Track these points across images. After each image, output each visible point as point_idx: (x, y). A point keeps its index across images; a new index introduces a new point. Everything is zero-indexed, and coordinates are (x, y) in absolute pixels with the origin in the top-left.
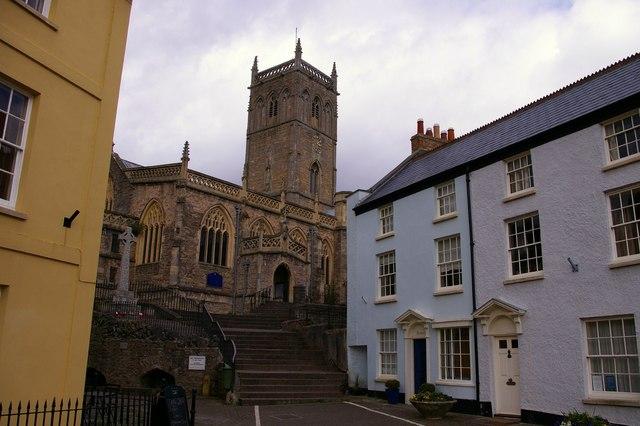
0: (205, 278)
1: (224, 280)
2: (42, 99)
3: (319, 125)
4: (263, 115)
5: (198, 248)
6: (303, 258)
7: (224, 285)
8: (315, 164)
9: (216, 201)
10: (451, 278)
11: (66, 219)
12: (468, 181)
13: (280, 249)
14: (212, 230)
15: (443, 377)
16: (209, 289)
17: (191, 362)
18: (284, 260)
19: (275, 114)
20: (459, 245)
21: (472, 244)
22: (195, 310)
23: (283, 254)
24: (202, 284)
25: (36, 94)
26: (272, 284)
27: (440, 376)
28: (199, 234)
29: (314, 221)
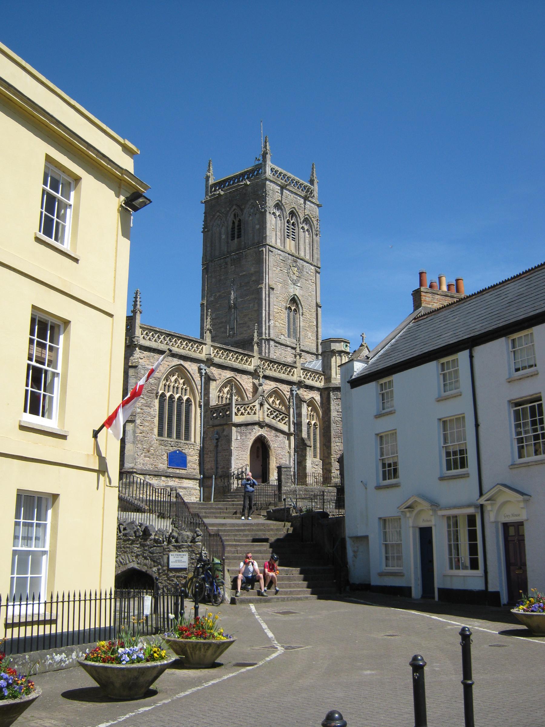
1: (189, 458)
2: (73, 327)
3: (298, 248)
4: (223, 237)
5: (156, 420)
6: (285, 428)
8: (294, 300)
9: (176, 362)
10: (456, 460)
11: (94, 431)
12: (471, 357)
13: (256, 418)
14: (171, 397)
15: (451, 568)
16: (170, 470)
17: (172, 559)
18: (258, 432)
19: (239, 236)
20: (464, 426)
21: (477, 425)
22: (167, 499)
23: (261, 425)
24: (163, 465)
25: (67, 323)
27: (156, 431)
28: (156, 402)
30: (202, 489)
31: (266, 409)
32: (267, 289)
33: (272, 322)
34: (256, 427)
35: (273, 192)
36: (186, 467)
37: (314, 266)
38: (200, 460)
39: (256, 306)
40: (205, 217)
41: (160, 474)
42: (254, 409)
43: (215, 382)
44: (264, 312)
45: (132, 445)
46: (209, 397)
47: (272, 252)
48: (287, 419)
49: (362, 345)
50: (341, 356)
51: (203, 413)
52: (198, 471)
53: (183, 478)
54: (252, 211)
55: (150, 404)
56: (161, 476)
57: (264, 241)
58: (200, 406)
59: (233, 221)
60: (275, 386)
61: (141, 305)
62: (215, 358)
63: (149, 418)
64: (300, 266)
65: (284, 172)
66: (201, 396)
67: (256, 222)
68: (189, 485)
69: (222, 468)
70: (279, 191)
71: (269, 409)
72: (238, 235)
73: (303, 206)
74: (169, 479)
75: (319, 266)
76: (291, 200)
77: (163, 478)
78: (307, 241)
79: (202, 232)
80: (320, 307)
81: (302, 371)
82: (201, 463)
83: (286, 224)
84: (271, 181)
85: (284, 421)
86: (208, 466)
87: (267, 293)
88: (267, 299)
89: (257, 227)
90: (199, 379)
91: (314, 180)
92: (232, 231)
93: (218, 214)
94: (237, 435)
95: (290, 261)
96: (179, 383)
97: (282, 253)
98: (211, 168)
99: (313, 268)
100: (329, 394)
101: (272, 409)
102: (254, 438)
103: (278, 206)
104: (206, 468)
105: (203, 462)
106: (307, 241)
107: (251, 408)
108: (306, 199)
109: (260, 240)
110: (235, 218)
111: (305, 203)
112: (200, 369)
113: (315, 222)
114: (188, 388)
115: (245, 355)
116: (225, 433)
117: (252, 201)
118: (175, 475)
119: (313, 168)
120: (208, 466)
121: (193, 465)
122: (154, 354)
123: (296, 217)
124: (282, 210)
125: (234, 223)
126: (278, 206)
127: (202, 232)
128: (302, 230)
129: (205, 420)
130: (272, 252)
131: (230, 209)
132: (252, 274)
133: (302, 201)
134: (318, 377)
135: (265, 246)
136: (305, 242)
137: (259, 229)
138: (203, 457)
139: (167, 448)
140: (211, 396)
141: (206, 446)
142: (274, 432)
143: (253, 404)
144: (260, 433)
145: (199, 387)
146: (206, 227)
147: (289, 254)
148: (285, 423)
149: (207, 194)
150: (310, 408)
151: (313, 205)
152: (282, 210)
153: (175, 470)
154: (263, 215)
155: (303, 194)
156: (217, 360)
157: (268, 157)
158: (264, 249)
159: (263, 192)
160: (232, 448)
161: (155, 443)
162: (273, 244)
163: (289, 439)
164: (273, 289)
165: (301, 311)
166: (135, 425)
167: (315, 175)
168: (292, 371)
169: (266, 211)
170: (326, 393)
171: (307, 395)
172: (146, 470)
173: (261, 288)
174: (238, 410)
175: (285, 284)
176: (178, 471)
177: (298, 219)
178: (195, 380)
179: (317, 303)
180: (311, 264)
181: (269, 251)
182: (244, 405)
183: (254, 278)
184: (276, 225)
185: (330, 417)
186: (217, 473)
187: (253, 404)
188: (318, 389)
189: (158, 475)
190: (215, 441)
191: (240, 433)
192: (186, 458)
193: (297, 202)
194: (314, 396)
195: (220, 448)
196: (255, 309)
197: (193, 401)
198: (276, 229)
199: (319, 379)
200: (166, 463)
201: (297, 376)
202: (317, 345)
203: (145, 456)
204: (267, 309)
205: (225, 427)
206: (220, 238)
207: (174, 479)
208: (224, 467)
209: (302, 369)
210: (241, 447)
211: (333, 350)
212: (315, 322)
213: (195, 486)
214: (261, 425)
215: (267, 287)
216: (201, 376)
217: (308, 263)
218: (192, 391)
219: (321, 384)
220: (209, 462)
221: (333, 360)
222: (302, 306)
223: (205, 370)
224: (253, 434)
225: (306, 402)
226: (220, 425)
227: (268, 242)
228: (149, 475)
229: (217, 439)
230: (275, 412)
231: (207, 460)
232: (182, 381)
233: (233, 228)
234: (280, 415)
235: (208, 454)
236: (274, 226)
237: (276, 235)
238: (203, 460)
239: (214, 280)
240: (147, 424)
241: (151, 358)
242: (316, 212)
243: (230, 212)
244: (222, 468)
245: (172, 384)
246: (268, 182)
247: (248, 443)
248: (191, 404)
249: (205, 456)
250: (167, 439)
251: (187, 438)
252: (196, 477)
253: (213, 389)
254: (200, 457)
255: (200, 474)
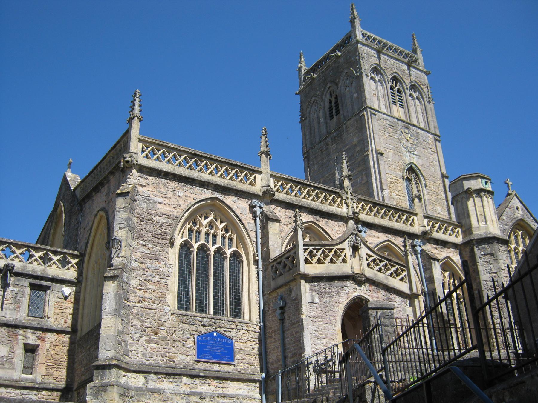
0: (190, 343)
1: (237, 346)
4: (322, 120)
5: (173, 282)
6: (404, 287)
7: (238, 357)
9: (208, 194)
16: (200, 366)
18: (352, 291)
19: (338, 113)
23: (358, 280)
24: (185, 356)
26: (339, 339)
27: (172, 299)
28: (173, 256)
29: (416, 229)
30: (264, 396)
31: (364, 256)
32: (375, 155)
33: (386, 192)
34: (349, 283)
35: (368, 57)
36: (233, 360)
37: (432, 134)
38: (260, 349)
39: (365, 178)
40: (301, 106)
41: (178, 371)
42: (343, 254)
43: (277, 224)
44: (374, 181)
45: (112, 318)
46: (268, 247)
47: (375, 115)
48: (405, 273)
49: (509, 194)
50: (481, 197)
51: (261, 273)
52: (258, 368)
53: (226, 379)
54: (348, 81)
55: (159, 255)
56: (180, 375)
57: (363, 104)
58: (256, 262)
59: (330, 100)
60: (385, 239)
61: (140, 111)
62: (276, 193)
63: (157, 278)
64: (414, 133)
65: (379, 38)
66: (257, 247)
67: (354, 91)
68: (240, 392)
69: (292, 357)
70: (376, 56)
71: (370, 256)
72: (336, 112)
73: (407, 72)
74: (197, 381)
75: (438, 133)
76: (390, 65)
77: (185, 379)
78: (419, 110)
79: (300, 123)
80: (447, 178)
81: (425, 220)
82: (263, 355)
83: (390, 91)
84: (364, 45)
85: (400, 277)
86: (274, 356)
87: (375, 159)
88: (376, 166)
89: (356, 95)
90: (253, 222)
91: (416, 49)
92: (330, 111)
93: (314, 98)
94: (312, 296)
95: (400, 127)
96: (217, 228)
97: (389, 118)
98: (303, 60)
99: (431, 136)
100: (472, 250)
101: (375, 256)
102: (347, 301)
103: (376, 70)
104: (271, 360)
105: (266, 352)
106: (419, 110)
107: (336, 252)
108: (409, 66)
109: (361, 104)
110: (331, 97)
111: (409, 69)
112: (252, 207)
113: (425, 90)
114: (235, 237)
115: (330, 192)
116: (293, 295)
117: (346, 71)
118: (213, 374)
119: (413, 39)
120: (274, 356)
121: (247, 357)
122: (166, 181)
123: (401, 83)
124: (381, 74)
125: (330, 102)
126: (376, 70)
127: (300, 123)
128: (410, 98)
129: (266, 282)
130: (375, 115)
131: (325, 88)
132: (356, 145)
133: (405, 67)
134: (452, 230)
135: (365, 109)
136: (416, 110)
137: (358, 98)
138: (265, 343)
139: (194, 328)
140: (270, 244)
141: (267, 323)
142: (383, 292)
143: (340, 247)
144: (357, 294)
145: (252, 234)
146: (303, 115)
147: (397, 119)
148: (402, 279)
149: (300, 85)
150: (447, 274)
151: (419, 73)
152: (381, 74)
153: (210, 365)
154: (359, 79)
155: (406, 60)
156: (280, 196)
157: (357, 21)
158: (365, 113)
159: (356, 56)
160: (303, 317)
161: (170, 321)
162: (376, 107)
163: (412, 305)
164: (382, 154)
165: (423, 182)
166: (119, 285)
167: (417, 45)
168: (411, 219)
169: (361, 73)
170: (468, 249)
171: (441, 253)
172: (150, 365)
173: (368, 155)
174: (311, 255)
175: (397, 151)
176: (216, 367)
177: (404, 85)
178: (245, 223)
179: (442, 174)
180: (428, 132)
181: (372, 113)
182: (323, 246)
183: (358, 149)
184: (377, 90)
185: (480, 282)
186: (285, 366)
187: (340, 247)
188: (455, 246)
189: (175, 375)
190: (279, 312)
191: (319, 292)
192: (232, 345)
193: (400, 67)
194: (451, 255)
195: (287, 323)
196: (363, 182)
197: (244, 255)
198: (378, 94)
199: (454, 232)
200: (193, 352)
201: (418, 226)
202: (448, 205)
203: (148, 341)
204: (378, 178)
205: (292, 284)
206: (319, 122)
207: (208, 381)
208: (295, 353)
209: (425, 217)
210: (324, 315)
211: (468, 189)
212: (444, 196)
213: (251, 394)
214: (358, 280)
215: (374, 153)
216: (255, 217)
217: (423, 130)
218: (241, 239)
219: (459, 239)
220: (274, 350)
221: (470, 203)
222: (423, 176)
223: (261, 208)
224: (343, 294)
225: (438, 260)
226: (286, 284)
227: (369, 104)
228: (156, 373)
229: (282, 308)
230: (381, 261)
231: (271, 346)
232: (222, 226)
233: (331, 108)
234: (392, 266)
235: (271, 337)
236: (374, 92)
237: (379, 100)
238: (265, 347)
239: (316, 167)
240: (153, 287)
241: (161, 186)
242: (424, 80)
243: (325, 92)
244: (292, 357)
245: (204, 230)
246: (359, 46)
247: (336, 309)
248: (242, 261)
249: (268, 341)
250: (194, 313)
251: (236, 311)
252: (253, 377)
253: (275, 234)
254: (260, 343)
255: (262, 371)
